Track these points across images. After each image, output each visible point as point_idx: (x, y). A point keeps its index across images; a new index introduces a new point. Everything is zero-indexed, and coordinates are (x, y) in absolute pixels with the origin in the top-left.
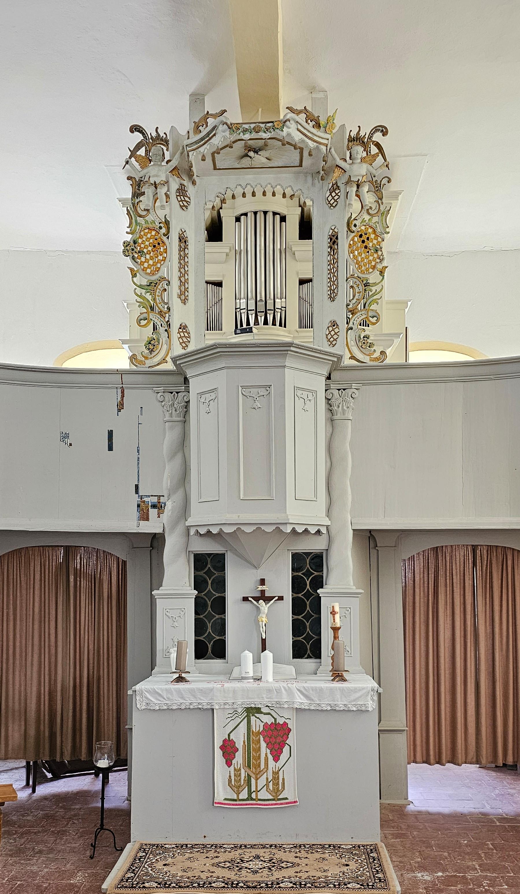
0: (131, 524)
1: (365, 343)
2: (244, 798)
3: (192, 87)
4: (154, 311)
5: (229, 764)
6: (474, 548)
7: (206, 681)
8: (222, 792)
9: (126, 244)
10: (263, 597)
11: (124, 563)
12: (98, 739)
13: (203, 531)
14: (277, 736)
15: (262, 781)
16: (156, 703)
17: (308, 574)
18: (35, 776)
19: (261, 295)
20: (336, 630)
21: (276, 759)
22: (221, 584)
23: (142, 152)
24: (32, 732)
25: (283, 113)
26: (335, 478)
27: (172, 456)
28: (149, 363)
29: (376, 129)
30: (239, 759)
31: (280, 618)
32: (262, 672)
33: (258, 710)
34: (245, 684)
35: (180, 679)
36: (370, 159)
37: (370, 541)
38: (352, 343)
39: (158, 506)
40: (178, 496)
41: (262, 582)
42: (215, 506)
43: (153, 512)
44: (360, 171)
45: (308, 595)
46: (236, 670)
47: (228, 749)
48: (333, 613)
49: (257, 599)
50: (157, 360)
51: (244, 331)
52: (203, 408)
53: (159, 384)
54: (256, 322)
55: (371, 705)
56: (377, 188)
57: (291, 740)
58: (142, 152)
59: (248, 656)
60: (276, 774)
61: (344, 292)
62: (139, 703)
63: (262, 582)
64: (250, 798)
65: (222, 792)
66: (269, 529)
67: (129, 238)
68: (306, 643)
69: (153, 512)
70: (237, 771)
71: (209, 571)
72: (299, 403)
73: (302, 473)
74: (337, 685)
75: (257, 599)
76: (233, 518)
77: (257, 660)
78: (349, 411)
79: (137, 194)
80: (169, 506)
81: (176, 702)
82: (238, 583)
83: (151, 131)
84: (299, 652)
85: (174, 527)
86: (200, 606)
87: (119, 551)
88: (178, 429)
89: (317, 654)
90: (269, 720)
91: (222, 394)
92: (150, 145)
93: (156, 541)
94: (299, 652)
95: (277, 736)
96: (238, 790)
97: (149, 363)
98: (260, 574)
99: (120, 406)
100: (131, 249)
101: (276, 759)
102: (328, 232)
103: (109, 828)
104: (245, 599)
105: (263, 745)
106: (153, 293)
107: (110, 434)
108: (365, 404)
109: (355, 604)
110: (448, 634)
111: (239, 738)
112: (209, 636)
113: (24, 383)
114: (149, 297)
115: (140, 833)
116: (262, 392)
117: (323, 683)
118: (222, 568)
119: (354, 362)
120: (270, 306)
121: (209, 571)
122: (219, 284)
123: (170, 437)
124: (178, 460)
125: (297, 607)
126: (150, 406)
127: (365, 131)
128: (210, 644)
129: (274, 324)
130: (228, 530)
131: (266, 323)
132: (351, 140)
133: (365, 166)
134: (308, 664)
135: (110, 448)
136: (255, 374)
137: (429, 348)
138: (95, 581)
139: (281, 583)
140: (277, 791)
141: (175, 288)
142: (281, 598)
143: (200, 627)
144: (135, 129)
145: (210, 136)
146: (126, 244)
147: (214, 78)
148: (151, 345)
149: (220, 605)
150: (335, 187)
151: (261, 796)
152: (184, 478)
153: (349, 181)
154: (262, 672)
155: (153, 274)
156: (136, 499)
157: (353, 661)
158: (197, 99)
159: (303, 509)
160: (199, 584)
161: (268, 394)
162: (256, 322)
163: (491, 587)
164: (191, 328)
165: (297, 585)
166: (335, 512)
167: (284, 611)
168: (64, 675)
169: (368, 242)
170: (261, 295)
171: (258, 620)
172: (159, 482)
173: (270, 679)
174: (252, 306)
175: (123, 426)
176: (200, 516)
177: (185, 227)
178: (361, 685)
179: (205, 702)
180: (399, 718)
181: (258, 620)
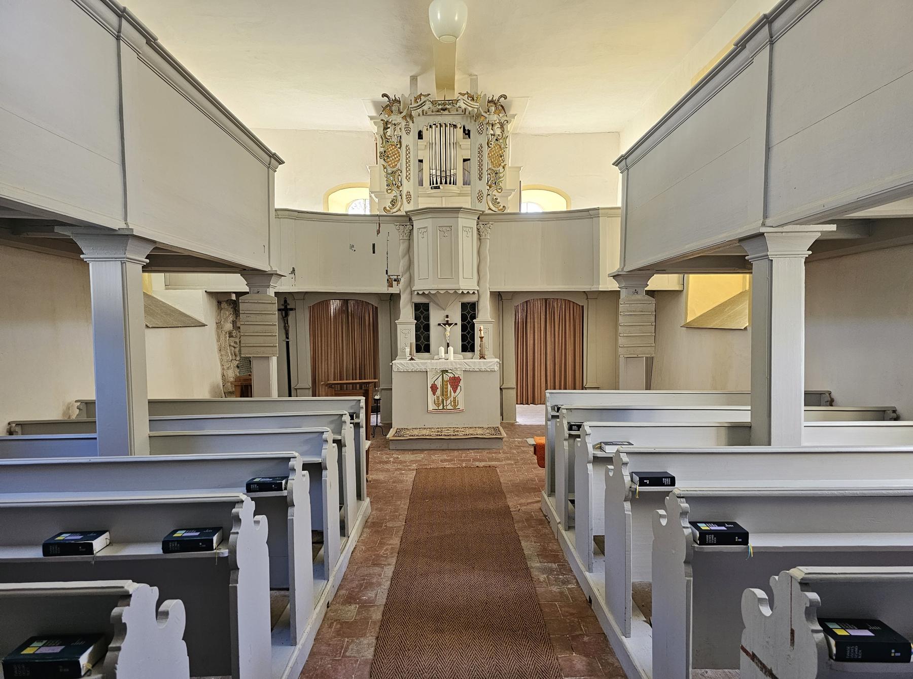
0: (384, 289)
1: (495, 201)
2: (441, 408)
4: (393, 181)
5: (434, 394)
6: (546, 300)
7: (422, 361)
8: (431, 407)
10: (448, 323)
11: (376, 308)
13: (421, 293)
14: (455, 382)
15: (449, 402)
16: (401, 368)
17: (469, 313)
20: (481, 338)
21: (455, 392)
22: (427, 318)
25: (456, 96)
26: (481, 267)
28: (392, 211)
29: (501, 96)
30: (439, 392)
31: (455, 333)
32: (447, 355)
33: (447, 371)
36: (497, 112)
37: (498, 297)
40: (407, 275)
41: (447, 316)
42: (426, 281)
43: (395, 283)
44: (494, 118)
45: (469, 323)
46: (436, 357)
47: (434, 388)
50: (395, 210)
51: (436, 188)
52: (421, 235)
53: (397, 221)
54: (441, 183)
55: (496, 368)
56: (502, 126)
57: (461, 384)
59: (442, 349)
60: (455, 398)
61: (485, 177)
62: (395, 369)
63: (447, 316)
65: (431, 407)
66: (452, 292)
69: (395, 283)
71: (422, 312)
73: (468, 269)
74: (482, 360)
77: (447, 352)
78: (488, 236)
79: (386, 128)
80: (402, 280)
81: (410, 368)
84: (464, 349)
85: (405, 291)
87: (374, 302)
88: (406, 243)
89: (473, 350)
90: (452, 376)
91: (430, 229)
92: (390, 105)
93: (394, 299)
94: (464, 349)
95: (455, 382)
97: (392, 211)
99: (378, 232)
101: (455, 392)
102: (478, 146)
106: (394, 177)
107: (374, 245)
108: (494, 231)
109: (490, 326)
110: (532, 342)
111: (439, 383)
112: (422, 323)
116: (448, 229)
117: (477, 360)
118: (428, 310)
119: (490, 212)
120: (448, 174)
121: (422, 312)
123: (403, 247)
124: (407, 257)
125: (464, 328)
126: (392, 231)
128: (423, 345)
130: (433, 292)
131: (446, 183)
132: (489, 102)
134: (469, 354)
136: (444, 221)
138: (362, 319)
140: (455, 406)
141: (404, 174)
147: (424, 70)
148: (393, 202)
149: (427, 328)
150: (481, 124)
152: (410, 265)
154: (447, 355)
155: (394, 167)
156: (386, 277)
157: (488, 353)
158: (414, 79)
159: (467, 283)
161: (450, 232)
162: (441, 183)
164: (412, 193)
165: (464, 318)
166: (482, 282)
169: (499, 141)
172: (397, 269)
174: (438, 173)
175: (380, 241)
176: (419, 286)
178: (492, 362)
179: (423, 368)
180: (511, 382)
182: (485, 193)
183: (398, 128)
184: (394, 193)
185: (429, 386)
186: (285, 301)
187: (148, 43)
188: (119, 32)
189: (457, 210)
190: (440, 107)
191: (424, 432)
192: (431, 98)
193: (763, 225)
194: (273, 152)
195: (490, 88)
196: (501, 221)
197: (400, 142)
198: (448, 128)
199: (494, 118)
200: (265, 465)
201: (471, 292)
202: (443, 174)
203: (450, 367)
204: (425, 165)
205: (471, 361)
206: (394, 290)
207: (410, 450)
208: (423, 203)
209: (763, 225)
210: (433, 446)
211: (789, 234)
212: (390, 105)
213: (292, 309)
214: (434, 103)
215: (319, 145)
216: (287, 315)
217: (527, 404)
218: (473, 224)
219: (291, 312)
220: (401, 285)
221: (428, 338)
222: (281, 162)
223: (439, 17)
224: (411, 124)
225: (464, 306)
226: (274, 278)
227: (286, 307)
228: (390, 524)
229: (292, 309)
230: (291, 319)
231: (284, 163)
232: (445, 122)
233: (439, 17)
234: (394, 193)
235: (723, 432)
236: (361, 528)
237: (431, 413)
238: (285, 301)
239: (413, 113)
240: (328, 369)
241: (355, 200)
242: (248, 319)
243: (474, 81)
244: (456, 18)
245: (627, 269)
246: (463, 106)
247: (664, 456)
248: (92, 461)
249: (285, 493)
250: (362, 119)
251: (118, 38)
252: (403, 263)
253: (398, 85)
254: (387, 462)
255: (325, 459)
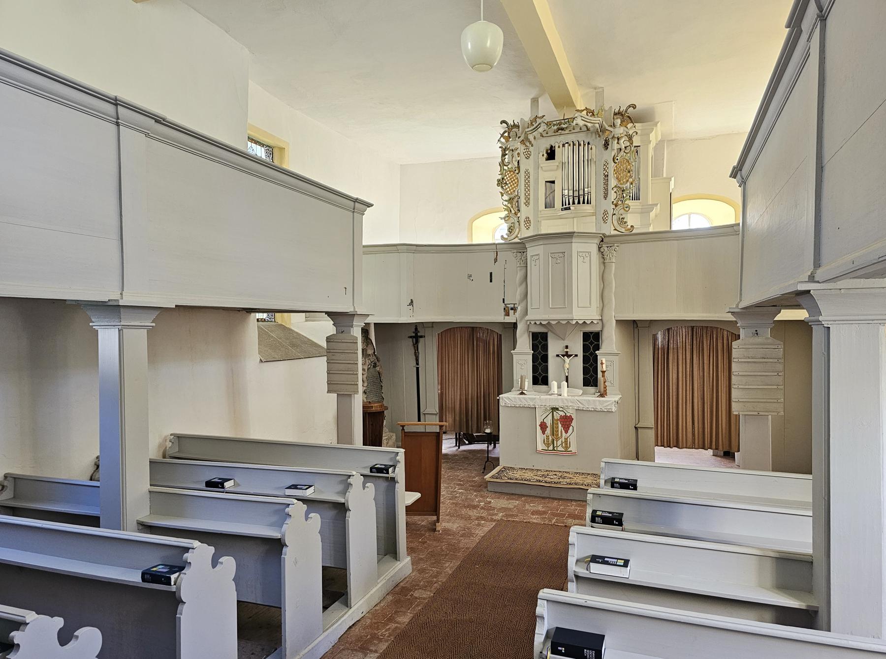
0: (500, 318)
3: (532, 96)
4: (513, 204)
5: (544, 433)
6: (693, 328)
7: (536, 396)
8: (540, 446)
9: (498, 180)
10: (568, 355)
12: (485, 420)
14: (567, 421)
15: (559, 442)
17: (591, 343)
18: (459, 442)
19: (576, 188)
20: (603, 372)
21: (566, 432)
23: (506, 134)
24: (457, 418)
26: (606, 293)
27: (521, 284)
29: (629, 106)
30: (548, 431)
31: (576, 366)
32: (565, 392)
33: (557, 409)
34: (552, 397)
35: (522, 393)
38: (615, 223)
39: (514, 309)
41: (567, 347)
42: (539, 312)
43: (511, 312)
47: (543, 426)
48: (602, 364)
49: (563, 356)
51: (566, 209)
54: (574, 203)
58: (506, 134)
61: (612, 196)
62: (502, 403)
63: (567, 347)
64: (554, 450)
67: (500, 177)
68: (591, 377)
69: (511, 312)
70: (548, 437)
71: (540, 341)
72: (581, 259)
75: (563, 356)
76: (546, 317)
78: (613, 257)
79: (504, 155)
81: (518, 404)
82: (554, 348)
83: (510, 122)
84: (586, 383)
85: (521, 320)
86: (535, 359)
87: (498, 330)
90: (562, 414)
91: (541, 257)
92: (511, 130)
93: (515, 325)
94: (586, 383)
95: (567, 421)
96: (548, 445)
98: (566, 343)
99: (496, 260)
100: (501, 183)
101: (566, 432)
102: (603, 162)
103: (491, 462)
104: (558, 356)
105: (560, 425)
106: (511, 203)
107: (491, 274)
110: (675, 376)
111: (548, 421)
113: (452, 252)
114: (509, 205)
115: (503, 463)
116: (561, 255)
118: (547, 340)
120: (581, 192)
121: (540, 341)
122: (553, 182)
123: (520, 275)
124: (524, 285)
126: (510, 258)
127: (623, 109)
128: (540, 378)
129: (584, 203)
131: (579, 203)
132: (615, 114)
133: (622, 128)
134: (591, 389)
135: (491, 281)
136: (557, 247)
137: (262, 504)
138: (486, 344)
139: (577, 347)
140: (566, 447)
142: (576, 356)
143: (535, 369)
144: (503, 122)
145: (537, 128)
146: (498, 180)
148: (511, 230)
149: (545, 359)
151: (559, 449)
153: (613, 137)
154: (565, 392)
156: (503, 306)
158: (535, 101)
159: (585, 310)
160: (534, 348)
161: (564, 258)
162: (574, 203)
163: (703, 350)
164: (531, 219)
167: (579, 362)
168: (472, 390)
170: (576, 188)
171: (565, 365)
172: (513, 298)
173: (566, 395)
174: (571, 193)
175: (497, 270)
177: (528, 167)
179: (531, 404)
181: (565, 365)
182: (611, 212)
183: (515, 153)
184: (512, 220)
185: (538, 423)
186: (416, 329)
187: (157, 121)
188: (118, 119)
189: (570, 235)
190: (556, 127)
191: (528, 475)
192: (547, 119)
193: (812, 279)
194: (356, 197)
195: (619, 97)
196: (628, 242)
197: (519, 167)
198: (581, 148)
199: (620, 131)
200: (168, 552)
201: (588, 322)
202: (576, 194)
203: (561, 404)
204: (557, 187)
205: (589, 398)
206: (511, 319)
207: (507, 494)
208: (547, 228)
209: (812, 279)
210: (533, 493)
211: (851, 292)
212: (511, 130)
213: (421, 337)
214: (548, 124)
215: (423, 181)
216: (417, 342)
217: (669, 446)
218: (593, 247)
219: (421, 340)
220: (517, 314)
221: (546, 370)
222: (370, 205)
223: (469, 47)
224: (531, 149)
225: (586, 336)
226: (356, 318)
227: (416, 334)
228: (416, 594)
229: (421, 337)
230: (420, 345)
231: (372, 205)
232: (578, 144)
233: (469, 47)
234: (512, 220)
235: (769, 565)
236: (384, 591)
237: (539, 453)
238: (416, 329)
239: (531, 137)
240: (455, 396)
241: (491, 229)
242: (334, 357)
243: (599, 93)
244: (488, 44)
245: (743, 305)
246: (581, 123)
247: (601, 614)
248: (44, 526)
249: (173, 588)
250: (489, 144)
251: (118, 124)
252: (520, 291)
253: (518, 110)
254: (475, 507)
255: (284, 535)
